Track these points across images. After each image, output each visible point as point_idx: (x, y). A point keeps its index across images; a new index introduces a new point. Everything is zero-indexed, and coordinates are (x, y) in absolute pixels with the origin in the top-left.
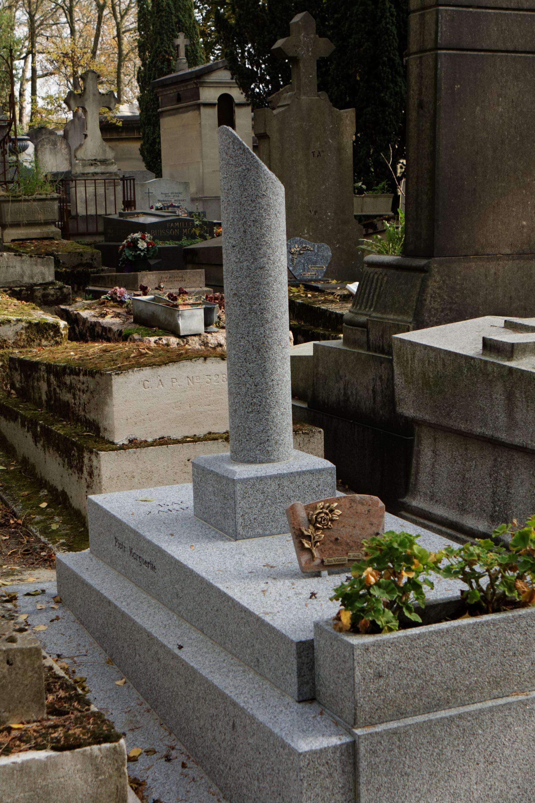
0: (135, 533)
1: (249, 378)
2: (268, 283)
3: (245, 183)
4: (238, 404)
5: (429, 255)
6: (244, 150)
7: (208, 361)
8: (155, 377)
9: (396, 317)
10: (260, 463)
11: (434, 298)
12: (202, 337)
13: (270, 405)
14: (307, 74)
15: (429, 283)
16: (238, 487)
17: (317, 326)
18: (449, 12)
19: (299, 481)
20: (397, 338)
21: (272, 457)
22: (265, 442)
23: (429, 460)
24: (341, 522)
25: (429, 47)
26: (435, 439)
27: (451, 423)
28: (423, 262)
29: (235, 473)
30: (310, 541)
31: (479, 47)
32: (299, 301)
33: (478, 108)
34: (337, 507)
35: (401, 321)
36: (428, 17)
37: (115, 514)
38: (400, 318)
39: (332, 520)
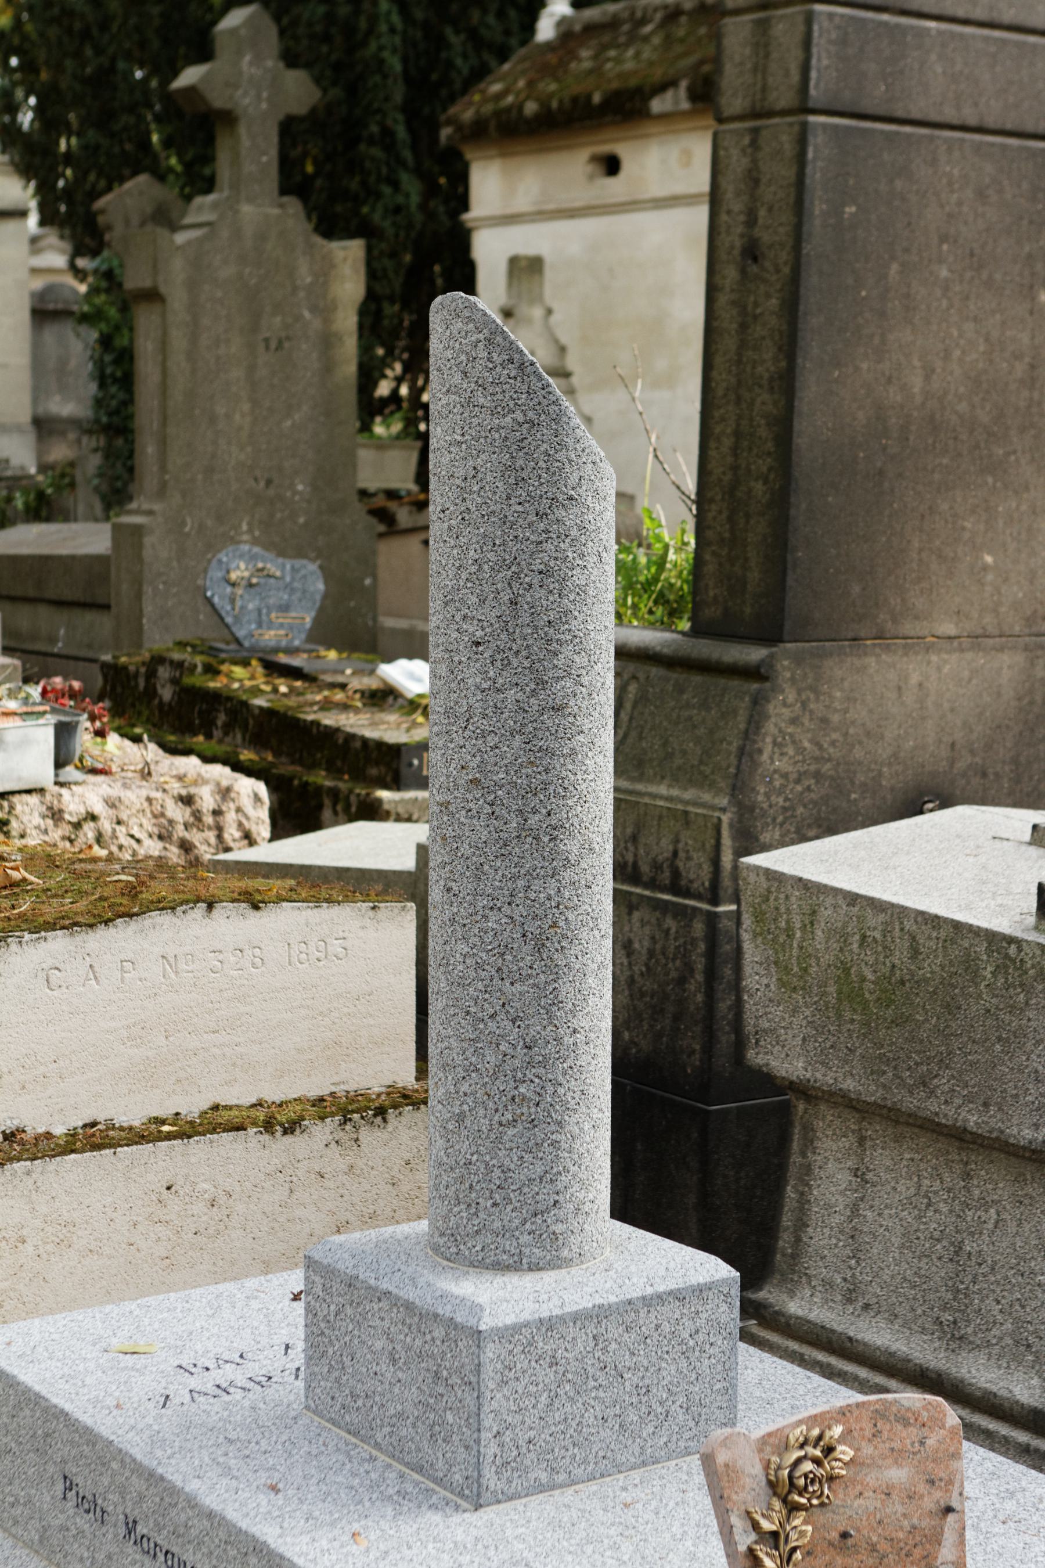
0: (153, 1478)
1: (509, 1025)
2: (574, 752)
3: (520, 462)
4: (470, 1100)
5: (770, 632)
6: (521, 367)
7: (218, 911)
8: (79, 957)
9: (675, 792)
10: (530, 1269)
11: (780, 746)
12: (48, 797)
13: (564, 1104)
14: (251, 154)
15: (770, 708)
16: (490, 1351)
17: (312, 766)
18: (837, 20)
19: (647, 1321)
20: (757, 868)
21: (565, 1253)
22: (548, 1210)
23: (842, 1193)
24: (853, 1481)
25: (782, 104)
26: (862, 1140)
27: (933, 1106)
28: (755, 654)
29: (476, 1309)
30: (777, 1548)
31: (900, 113)
32: (260, 702)
33: (895, 267)
34: (842, 1439)
35: (695, 804)
36: (779, 29)
37: (68, 1407)
38: (689, 795)
39: (831, 1478)
